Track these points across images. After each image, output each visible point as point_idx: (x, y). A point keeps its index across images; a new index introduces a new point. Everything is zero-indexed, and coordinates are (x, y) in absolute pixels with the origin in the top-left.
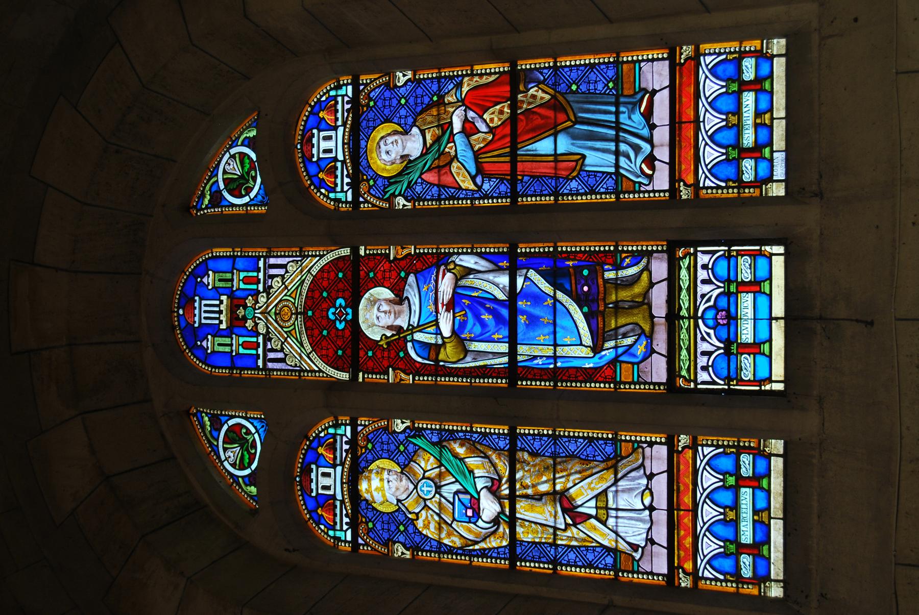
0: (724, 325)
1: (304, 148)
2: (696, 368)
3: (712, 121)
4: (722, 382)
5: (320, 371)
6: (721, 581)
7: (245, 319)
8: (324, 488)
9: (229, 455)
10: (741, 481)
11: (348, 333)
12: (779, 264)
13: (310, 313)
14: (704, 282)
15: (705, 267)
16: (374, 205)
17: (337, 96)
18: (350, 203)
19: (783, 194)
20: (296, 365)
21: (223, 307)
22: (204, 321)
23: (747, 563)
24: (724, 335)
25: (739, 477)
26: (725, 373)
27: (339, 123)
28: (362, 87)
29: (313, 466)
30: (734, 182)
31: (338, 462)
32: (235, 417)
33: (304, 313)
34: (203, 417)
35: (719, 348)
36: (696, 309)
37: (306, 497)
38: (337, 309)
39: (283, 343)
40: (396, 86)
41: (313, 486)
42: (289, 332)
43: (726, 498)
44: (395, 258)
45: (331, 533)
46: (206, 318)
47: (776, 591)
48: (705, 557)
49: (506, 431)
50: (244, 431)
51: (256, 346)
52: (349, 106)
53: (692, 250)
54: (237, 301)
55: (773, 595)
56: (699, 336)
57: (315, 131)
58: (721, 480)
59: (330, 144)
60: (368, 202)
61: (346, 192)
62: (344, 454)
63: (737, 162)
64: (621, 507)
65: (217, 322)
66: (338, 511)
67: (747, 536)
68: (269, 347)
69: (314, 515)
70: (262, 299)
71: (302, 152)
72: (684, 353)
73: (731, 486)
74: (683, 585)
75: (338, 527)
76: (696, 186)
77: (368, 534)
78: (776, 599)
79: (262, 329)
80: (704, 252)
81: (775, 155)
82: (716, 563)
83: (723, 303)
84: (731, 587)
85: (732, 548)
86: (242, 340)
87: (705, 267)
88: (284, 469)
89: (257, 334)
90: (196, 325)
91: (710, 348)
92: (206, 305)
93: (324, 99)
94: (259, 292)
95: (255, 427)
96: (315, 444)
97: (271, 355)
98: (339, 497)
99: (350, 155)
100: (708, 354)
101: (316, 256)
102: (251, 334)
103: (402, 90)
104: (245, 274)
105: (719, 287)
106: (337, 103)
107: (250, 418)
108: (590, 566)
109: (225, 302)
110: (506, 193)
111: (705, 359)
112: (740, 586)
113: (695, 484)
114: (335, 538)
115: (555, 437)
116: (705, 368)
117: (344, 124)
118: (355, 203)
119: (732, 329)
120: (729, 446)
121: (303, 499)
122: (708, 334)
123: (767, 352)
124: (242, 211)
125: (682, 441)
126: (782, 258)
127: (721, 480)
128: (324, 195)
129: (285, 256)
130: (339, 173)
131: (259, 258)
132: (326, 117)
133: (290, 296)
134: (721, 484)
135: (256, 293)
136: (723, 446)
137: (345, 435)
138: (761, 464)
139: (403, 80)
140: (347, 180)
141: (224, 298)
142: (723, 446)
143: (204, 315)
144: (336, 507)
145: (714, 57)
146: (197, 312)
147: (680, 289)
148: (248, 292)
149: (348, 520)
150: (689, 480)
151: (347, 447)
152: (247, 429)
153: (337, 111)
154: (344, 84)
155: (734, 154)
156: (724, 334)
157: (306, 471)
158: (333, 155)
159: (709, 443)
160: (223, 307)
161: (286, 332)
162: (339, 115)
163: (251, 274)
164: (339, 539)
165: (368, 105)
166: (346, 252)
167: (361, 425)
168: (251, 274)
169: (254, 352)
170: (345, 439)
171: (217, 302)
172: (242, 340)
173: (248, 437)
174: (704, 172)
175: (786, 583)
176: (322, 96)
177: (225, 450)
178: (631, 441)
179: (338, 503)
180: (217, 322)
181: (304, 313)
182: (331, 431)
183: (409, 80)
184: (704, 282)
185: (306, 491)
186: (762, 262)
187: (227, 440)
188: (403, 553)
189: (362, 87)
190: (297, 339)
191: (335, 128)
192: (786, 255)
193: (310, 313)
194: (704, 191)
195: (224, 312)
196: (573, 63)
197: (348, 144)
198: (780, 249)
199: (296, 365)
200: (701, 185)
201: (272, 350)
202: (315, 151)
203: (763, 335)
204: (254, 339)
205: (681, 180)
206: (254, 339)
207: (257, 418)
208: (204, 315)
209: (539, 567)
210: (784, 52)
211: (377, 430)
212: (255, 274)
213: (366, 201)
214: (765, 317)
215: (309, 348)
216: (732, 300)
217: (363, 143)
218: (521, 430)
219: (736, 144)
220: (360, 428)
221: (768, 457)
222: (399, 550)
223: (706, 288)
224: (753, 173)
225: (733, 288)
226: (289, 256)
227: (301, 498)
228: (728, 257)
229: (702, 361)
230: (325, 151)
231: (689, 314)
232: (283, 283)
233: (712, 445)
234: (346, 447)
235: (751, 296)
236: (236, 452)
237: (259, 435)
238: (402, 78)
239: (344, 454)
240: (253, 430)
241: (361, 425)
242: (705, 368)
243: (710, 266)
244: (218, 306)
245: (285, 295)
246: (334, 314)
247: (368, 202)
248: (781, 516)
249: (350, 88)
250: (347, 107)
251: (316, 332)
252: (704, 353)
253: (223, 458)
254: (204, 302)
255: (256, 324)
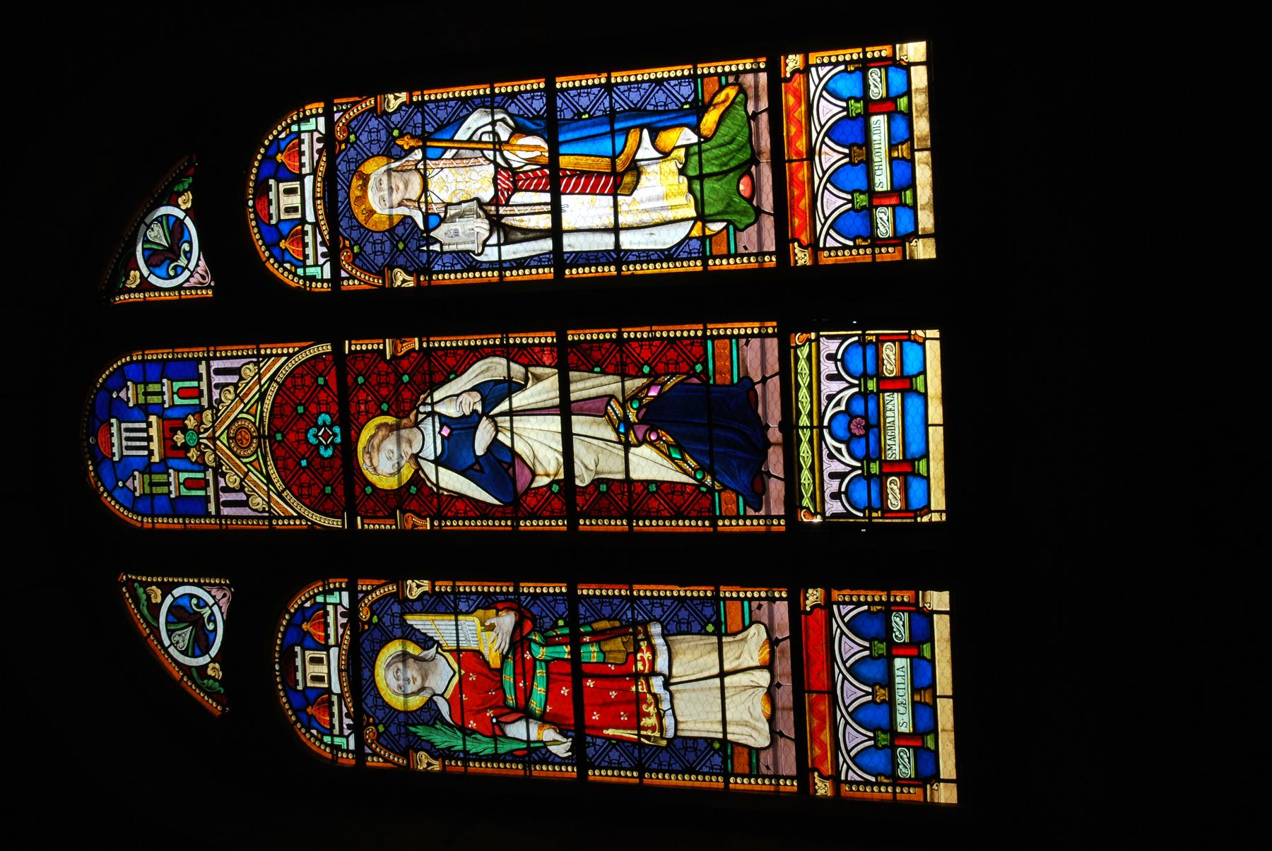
0: (861, 436)
1: (259, 207)
2: (822, 492)
3: (852, 693)
4: (861, 515)
5: (300, 517)
6: (850, 248)
7: (186, 447)
8: (315, 678)
9: (174, 646)
10: (871, 107)
11: (338, 463)
12: (933, 350)
13: (279, 437)
14: (831, 378)
15: (831, 357)
16: (386, 760)
17: (325, 604)
18: (327, 281)
19: (934, 256)
20: (264, 511)
21: (153, 432)
22: (126, 453)
23: (885, 218)
24: (860, 451)
25: (891, 644)
26: (860, 368)
27: (306, 170)
28: (360, 596)
29: (298, 649)
30: (865, 240)
31: (332, 641)
32: (183, 584)
33: (271, 437)
34: (135, 589)
35: (854, 468)
36: (821, 418)
37: (264, 228)
38: (320, 443)
39: (242, 480)
40: (385, 113)
41: (299, 676)
42: (250, 463)
43: (876, 671)
44: (393, 356)
45: (327, 739)
46: (128, 448)
47: (946, 794)
48: (822, 127)
49: (564, 590)
50: (194, 601)
51: (203, 484)
52: (321, 146)
53: (813, 336)
54: (172, 425)
55: (943, 801)
56: (825, 452)
57: (272, 182)
58: (849, 201)
59: (323, 669)
60: (379, 755)
61: (322, 266)
62: (316, 156)
63: (868, 213)
64: (725, 649)
65: (146, 453)
66: (335, 710)
67: (904, 722)
68: (222, 484)
69: (276, 252)
70: (208, 415)
71: (255, 212)
72: (803, 392)
73: (881, 656)
74: (800, 263)
75: (336, 731)
76: (835, 779)
77: (377, 740)
78: (947, 807)
79: (210, 459)
80: (828, 337)
81: (917, 155)
82: (865, 760)
83: (858, 407)
84: (885, 792)
85: (881, 648)
86: (183, 476)
87: (831, 357)
88: (258, 643)
89: (205, 468)
90: (116, 459)
91: (840, 468)
92: (127, 430)
93: (283, 135)
94: (202, 409)
95: (214, 597)
96: (297, 619)
97: (224, 497)
98: (310, 217)
99: (349, 682)
100: (839, 476)
101: (283, 355)
102: (196, 468)
103: (396, 118)
104: (186, 475)
105: (852, 386)
106: (327, 613)
107: (205, 584)
108: (659, 82)
109: (155, 424)
110: (562, 511)
111: (836, 483)
112: (898, 790)
113: (836, 747)
114: (305, 278)
115: (609, 87)
116: (835, 496)
117: (314, 172)
118: (336, 279)
119: (872, 439)
120: (874, 603)
121: (259, 232)
122: (839, 450)
123: (909, 201)
124: (174, 296)
125: (811, 599)
126: (941, 429)
127: (849, 201)
128: (290, 272)
129: (237, 357)
130: (309, 239)
131: (199, 360)
132: (291, 248)
133: (247, 413)
134: (850, 206)
135: (199, 410)
136: (866, 603)
137: (341, 604)
138: (897, 78)
139: (416, 593)
140: (322, 249)
141: (153, 419)
142: (866, 603)
143: (125, 435)
144: (332, 703)
145: (828, 68)
146: (115, 440)
147: (798, 387)
148: (189, 411)
149: (325, 250)
150: (822, 649)
151: (345, 620)
152: (198, 598)
153: (327, 625)
154: (312, 116)
155: (862, 200)
156: (859, 448)
157: (288, 657)
158: (298, 216)
159: (826, 61)
160: (153, 432)
161: (245, 464)
162: (331, 631)
163: (187, 384)
164: (339, 748)
165: (347, 140)
166: (328, 348)
167: (362, 591)
168: (187, 384)
169: (201, 493)
170: (340, 609)
171: (144, 425)
172: (183, 476)
173: (203, 611)
174: (843, 716)
175: (961, 782)
176: (280, 133)
177: (170, 633)
178: (716, 74)
179: (335, 699)
180: (146, 453)
181: (271, 437)
182: (295, 128)
183: (424, 593)
184: (831, 378)
185: (290, 682)
186: (912, 351)
187: (171, 618)
188: (429, 764)
189: (360, 596)
190: (261, 473)
191: (327, 648)
192: (941, 339)
193: (279, 437)
194: (826, 253)
195: (155, 439)
196: (632, 79)
197: (322, 198)
198: (934, 333)
199: (264, 511)
200: (843, 778)
201: (227, 489)
202: (273, 210)
203: (915, 448)
204: (200, 475)
205: (793, 241)
206: (200, 475)
207: (215, 584)
208: (125, 443)
209: (626, 776)
210: (954, 777)
211: (384, 597)
212: (195, 384)
213: (374, 754)
214: (920, 421)
215: (280, 485)
216: (872, 405)
217: (366, 674)
218: (562, 82)
219: (891, 728)
220: (337, 116)
221: (906, 68)
222: (401, 278)
223: (835, 386)
224: (891, 226)
225: (873, 383)
226: (243, 357)
227: (256, 230)
228: (862, 343)
229: (832, 486)
230: (288, 210)
231: (812, 422)
232: (237, 395)
233: (851, 603)
234: (343, 620)
235: (897, 397)
236: (186, 625)
237: (220, 608)
238: (393, 101)
239: (341, 631)
240: (211, 601)
241: (338, 111)
242: (835, 496)
243: (839, 357)
244: (146, 430)
245: (241, 412)
246: (316, 436)
247: (379, 755)
248: (950, 693)
249: (322, 120)
250: (343, 620)
251: (291, 463)
252: (833, 476)
253: (167, 642)
254: (124, 425)
255: (203, 454)
